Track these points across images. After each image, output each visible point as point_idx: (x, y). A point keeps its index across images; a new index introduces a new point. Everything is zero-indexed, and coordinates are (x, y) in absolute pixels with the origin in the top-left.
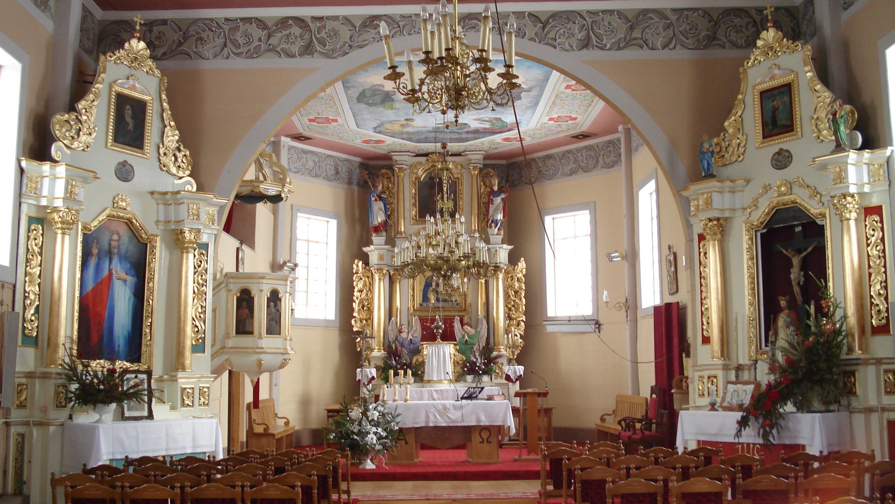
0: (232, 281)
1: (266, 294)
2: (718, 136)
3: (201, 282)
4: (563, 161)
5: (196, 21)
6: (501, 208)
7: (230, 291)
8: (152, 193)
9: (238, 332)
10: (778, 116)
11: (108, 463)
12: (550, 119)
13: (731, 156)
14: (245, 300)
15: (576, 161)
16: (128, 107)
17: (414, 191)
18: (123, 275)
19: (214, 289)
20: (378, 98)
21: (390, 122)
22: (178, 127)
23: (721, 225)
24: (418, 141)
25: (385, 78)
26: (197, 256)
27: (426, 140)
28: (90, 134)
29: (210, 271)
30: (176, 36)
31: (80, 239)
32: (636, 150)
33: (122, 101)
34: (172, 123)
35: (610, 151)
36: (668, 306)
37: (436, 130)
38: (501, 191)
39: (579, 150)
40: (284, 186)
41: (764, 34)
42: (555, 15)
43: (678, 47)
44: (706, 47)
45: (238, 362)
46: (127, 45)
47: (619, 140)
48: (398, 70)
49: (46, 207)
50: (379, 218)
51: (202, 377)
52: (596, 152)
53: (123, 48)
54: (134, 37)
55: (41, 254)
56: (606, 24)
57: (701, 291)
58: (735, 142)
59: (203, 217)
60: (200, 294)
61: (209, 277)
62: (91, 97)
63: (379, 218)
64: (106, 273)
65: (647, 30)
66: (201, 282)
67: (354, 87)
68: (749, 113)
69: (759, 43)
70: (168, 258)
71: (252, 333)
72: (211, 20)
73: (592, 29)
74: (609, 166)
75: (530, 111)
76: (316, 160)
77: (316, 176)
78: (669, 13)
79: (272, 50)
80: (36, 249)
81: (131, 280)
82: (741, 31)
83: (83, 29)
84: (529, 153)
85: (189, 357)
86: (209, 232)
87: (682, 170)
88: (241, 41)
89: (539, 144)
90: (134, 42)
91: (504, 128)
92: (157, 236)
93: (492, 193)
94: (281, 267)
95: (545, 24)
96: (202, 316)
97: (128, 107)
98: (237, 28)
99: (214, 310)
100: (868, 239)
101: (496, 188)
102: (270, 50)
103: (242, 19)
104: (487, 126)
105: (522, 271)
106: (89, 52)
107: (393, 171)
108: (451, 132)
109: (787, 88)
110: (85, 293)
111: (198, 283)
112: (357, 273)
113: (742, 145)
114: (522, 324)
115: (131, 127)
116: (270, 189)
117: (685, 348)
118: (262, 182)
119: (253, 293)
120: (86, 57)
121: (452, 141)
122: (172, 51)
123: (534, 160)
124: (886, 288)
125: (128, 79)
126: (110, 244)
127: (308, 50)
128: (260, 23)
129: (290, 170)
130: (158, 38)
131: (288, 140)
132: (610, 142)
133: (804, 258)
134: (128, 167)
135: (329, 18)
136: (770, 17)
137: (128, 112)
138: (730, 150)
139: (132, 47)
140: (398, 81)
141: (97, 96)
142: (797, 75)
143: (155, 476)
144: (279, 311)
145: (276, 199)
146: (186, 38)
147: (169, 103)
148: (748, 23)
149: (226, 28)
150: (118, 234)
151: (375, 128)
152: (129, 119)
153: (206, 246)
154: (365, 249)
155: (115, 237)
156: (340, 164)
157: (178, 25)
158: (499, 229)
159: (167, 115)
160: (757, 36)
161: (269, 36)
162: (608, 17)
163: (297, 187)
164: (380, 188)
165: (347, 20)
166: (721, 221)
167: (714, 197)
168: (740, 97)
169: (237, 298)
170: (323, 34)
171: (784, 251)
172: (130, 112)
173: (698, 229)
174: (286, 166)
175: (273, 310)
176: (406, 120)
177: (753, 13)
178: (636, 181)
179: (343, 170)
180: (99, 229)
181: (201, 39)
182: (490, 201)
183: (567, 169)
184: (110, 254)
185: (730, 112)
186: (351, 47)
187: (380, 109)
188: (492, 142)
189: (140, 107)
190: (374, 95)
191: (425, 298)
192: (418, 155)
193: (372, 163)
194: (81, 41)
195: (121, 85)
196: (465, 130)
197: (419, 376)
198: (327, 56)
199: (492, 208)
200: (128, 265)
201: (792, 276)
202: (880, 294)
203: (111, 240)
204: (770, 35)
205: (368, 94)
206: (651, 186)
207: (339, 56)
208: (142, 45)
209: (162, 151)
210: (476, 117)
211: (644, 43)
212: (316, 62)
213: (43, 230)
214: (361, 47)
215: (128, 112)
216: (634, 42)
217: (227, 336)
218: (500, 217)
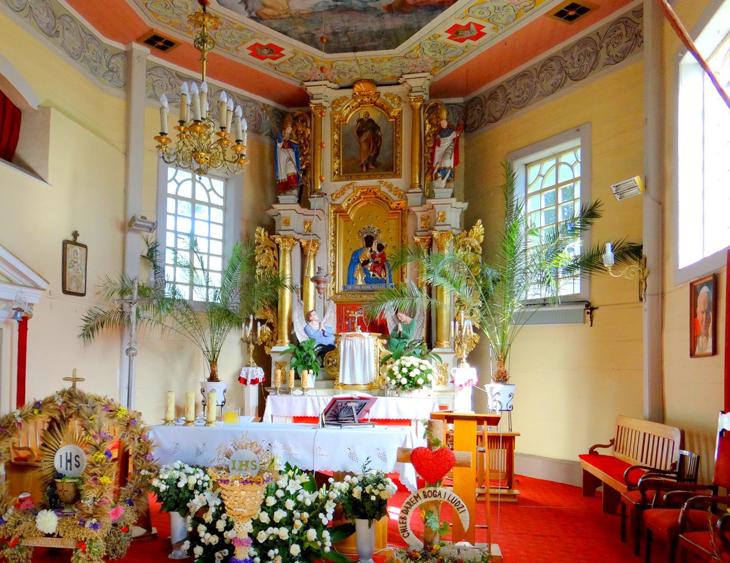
4: (542, 75)
15: (562, 68)
17: (336, 137)
25: (284, 49)
35: (620, 35)
39: (565, 52)
50: (287, 167)
84: (480, 83)
93: (441, 132)
101: (444, 124)
105: (478, 239)
112: (259, 244)
114: (477, 311)
123: (501, 87)
158: (448, 181)
182: (437, 143)
183: (548, 85)
191: (350, 279)
192: (341, 88)
199: (439, 151)
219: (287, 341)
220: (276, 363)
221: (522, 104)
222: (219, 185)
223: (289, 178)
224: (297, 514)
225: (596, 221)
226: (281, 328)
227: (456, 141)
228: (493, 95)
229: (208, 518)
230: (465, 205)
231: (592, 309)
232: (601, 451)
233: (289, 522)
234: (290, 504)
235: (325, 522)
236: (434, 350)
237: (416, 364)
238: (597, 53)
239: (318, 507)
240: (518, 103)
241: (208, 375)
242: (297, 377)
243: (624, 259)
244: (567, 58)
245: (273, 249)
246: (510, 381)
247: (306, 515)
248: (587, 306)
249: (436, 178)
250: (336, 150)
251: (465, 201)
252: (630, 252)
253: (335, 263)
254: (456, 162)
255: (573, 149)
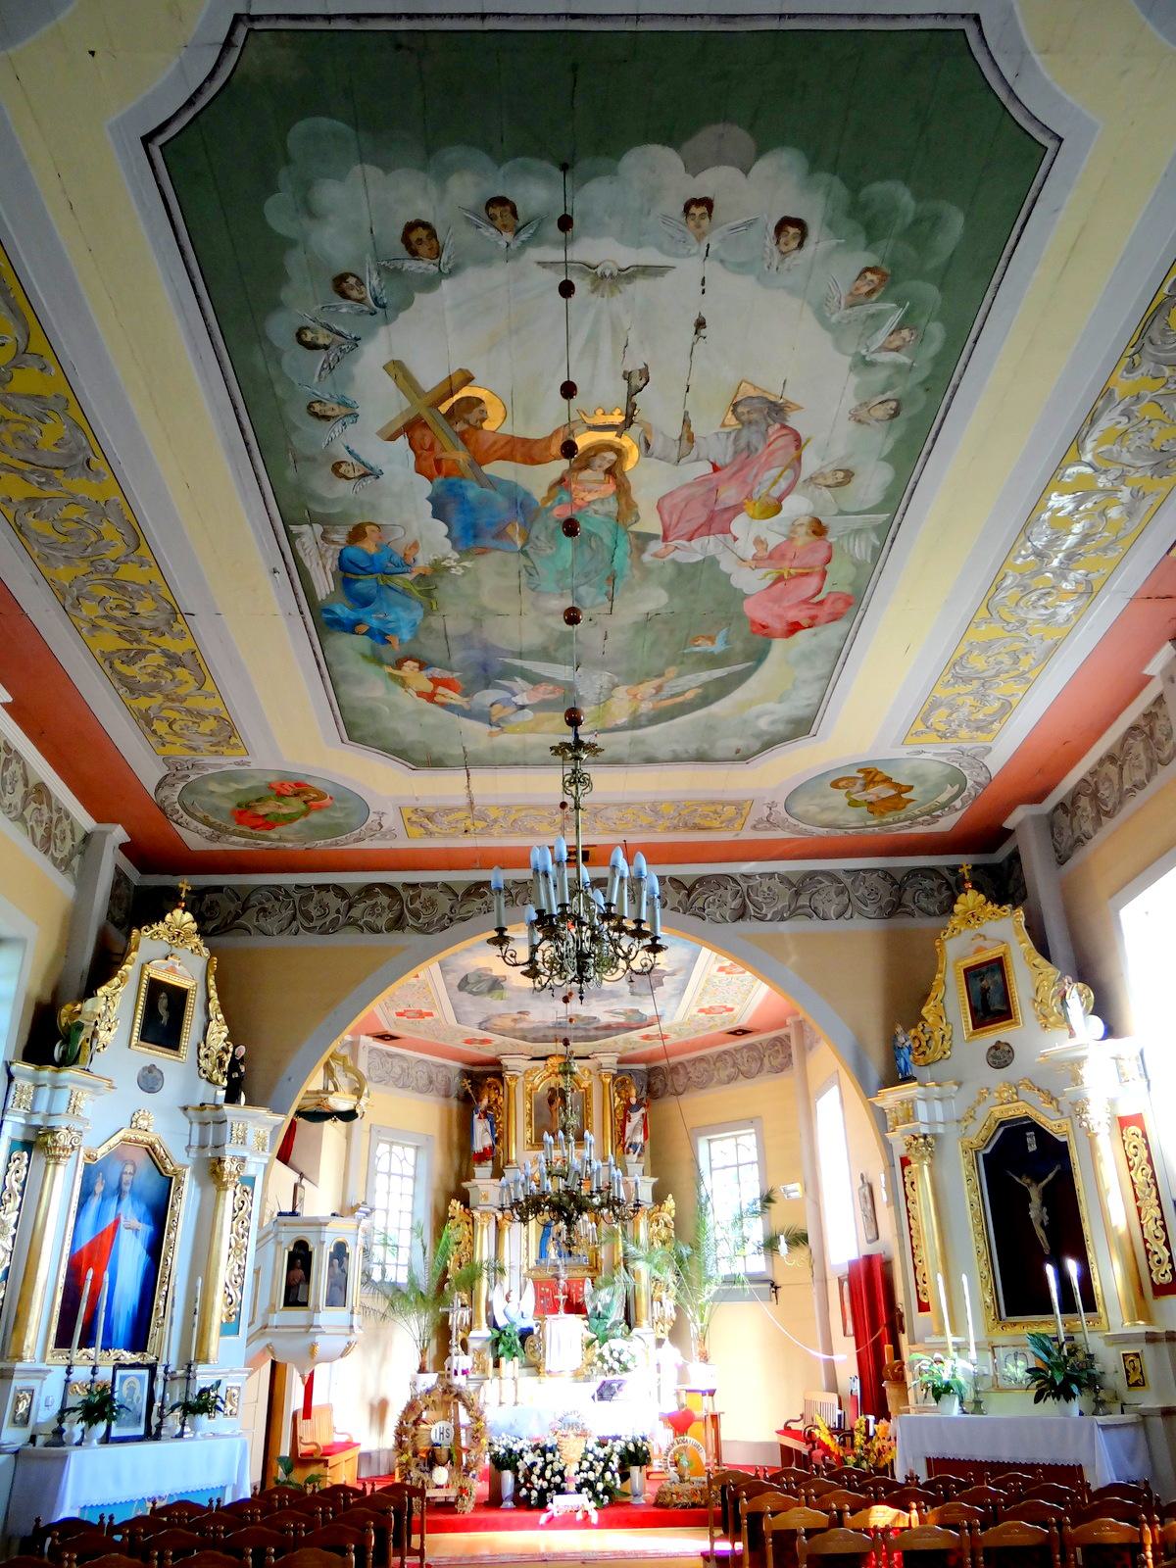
0: (283, 1229)
1: (329, 1248)
2: (916, 1027)
3: (241, 1231)
5: (258, 888)
6: (640, 1127)
7: (280, 1243)
8: (185, 1109)
9: (285, 1305)
10: (991, 1002)
11: (76, 1514)
12: (702, 1011)
13: (934, 1052)
14: (301, 1257)
15: (735, 1065)
16: (163, 995)
17: (528, 1106)
18: (135, 1223)
19: (258, 1242)
20: (484, 986)
21: (500, 1016)
22: (228, 1021)
23: (930, 1145)
24: (535, 1040)
26: (239, 1195)
27: (545, 1039)
28: (109, 1029)
29: (255, 1216)
30: (233, 907)
31: (80, 1173)
32: (810, 1049)
33: (156, 987)
34: (220, 1016)
35: (778, 1051)
36: (869, 1259)
37: (558, 1026)
38: (639, 1105)
40: (359, 1098)
41: (962, 898)
42: (701, 880)
43: (856, 915)
44: (890, 915)
45: (285, 1348)
46: (168, 916)
47: (788, 1037)
48: (506, 934)
49: (39, 1128)
51: (231, 1371)
52: (762, 1051)
53: (163, 921)
54: (178, 907)
55: (22, 1195)
56: (766, 889)
57: (911, 1237)
58: (937, 1035)
59: (251, 1139)
60: (238, 1249)
61: (253, 1224)
62: (116, 981)
63: (482, 1139)
64: (111, 1220)
65: (816, 896)
66: (241, 1231)
67: (454, 971)
68: (952, 1001)
69: (957, 908)
70: (198, 1197)
71: (305, 1304)
72: (279, 887)
73: (748, 894)
74: (779, 1070)
75: (674, 1001)
76: (405, 1065)
77: (404, 1087)
78: (842, 876)
79: (352, 923)
80: (17, 1186)
81: (146, 1229)
82: (933, 895)
83: (114, 897)
84: (673, 1055)
85: (215, 1342)
86: (258, 1160)
87: (875, 1069)
88: (314, 913)
89: (687, 1042)
90: (178, 912)
91: (642, 1023)
92: (186, 1167)
93: (628, 1108)
94: (353, 1210)
95: (690, 891)
96: (239, 1280)
97: (163, 995)
98: (310, 898)
99: (257, 1272)
100: (1128, 1159)
101: (633, 1101)
102: (349, 924)
103: (317, 887)
104: (622, 1019)
106: (118, 925)
107: (502, 1080)
108: (576, 1029)
109: (998, 965)
110: (77, 1249)
111: (238, 1234)
113: (947, 1037)
115: (164, 1021)
116: (341, 1102)
117: (895, 1324)
118: (332, 1093)
119: (311, 1247)
120: (113, 930)
121: (577, 1039)
122: (226, 925)
123: (681, 1063)
124: (1164, 1227)
125: (166, 959)
126: (121, 1179)
127: (397, 924)
128: (339, 890)
129: (371, 1079)
130: (209, 909)
131: (370, 1039)
132: (777, 1039)
133: (1044, 1188)
134: (155, 1073)
135: (424, 885)
136: (967, 877)
137: (163, 1002)
138: (932, 1044)
139: (175, 919)
140: (504, 948)
141: (123, 979)
142: (1008, 948)
143: (179, 1517)
144: (344, 1272)
145: (349, 1116)
146: (245, 909)
147: (218, 991)
148: (941, 885)
149: (297, 896)
150: (134, 1164)
151: (480, 1023)
152: (162, 1011)
153: (251, 1181)
154: (465, 1185)
155: (129, 1169)
156: (434, 1070)
157: (235, 892)
158: (639, 1155)
159: (214, 1004)
160: (954, 900)
161: (350, 907)
162: (767, 882)
163: (380, 1104)
164: (485, 1102)
165: (447, 887)
166: (929, 1139)
167: (923, 1103)
168: (938, 976)
169: (290, 1253)
170: (417, 905)
171: (1017, 1179)
172: (165, 1002)
173: (900, 1150)
174: (366, 1075)
175: (337, 1270)
176: (520, 1013)
177: (946, 873)
178: (812, 1088)
179: (440, 1080)
180: (108, 1158)
181: (264, 910)
182: (627, 1118)
183: (724, 1074)
184: (119, 1192)
185: (927, 995)
186: (451, 920)
187: (487, 999)
188: (627, 1041)
189: (178, 997)
190: (479, 982)
191: (543, 1252)
192: (534, 1059)
193: (477, 1069)
194: (109, 912)
195: (156, 968)
196: (595, 1025)
197: (535, 1367)
198: (420, 930)
199: (629, 1127)
200: (143, 1208)
201: (1032, 1214)
202: (1157, 1237)
203: (122, 1173)
204: (970, 899)
205: (471, 980)
206: (833, 1093)
207: (436, 930)
208: (188, 916)
209: (202, 1052)
210: (607, 1009)
211: (814, 912)
212: (408, 939)
213: (29, 1159)
214: (464, 920)
215: (163, 1002)
216: (800, 911)
217: (272, 1308)
218: (639, 1138)
219: (484, 1324)
220: (474, 1350)
221: (702, 1086)
222: (410, 1153)
223: (485, 1149)
224: (595, 1463)
225: (772, 1205)
226: (479, 1310)
227: (644, 1116)
228: (674, 1069)
229: (537, 1471)
230: (654, 1180)
231: (776, 1288)
232: (794, 1426)
233: (592, 1468)
234: (590, 1457)
235: (614, 1469)
236: (635, 1331)
237: (625, 1349)
238: (762, 1060)
239: (607, 1460)
240: (698, 1083)
241: (418, 1368)
242: (497, 1365)
243: (797, 1244)
244: (738, 1056)
245: (468, 1224)
246: (710, 1361)
247: (602, 1464)
248: (772, 1285)
249: (628, 1153)
250: (528, 1118)
251: (653, 1175)
252: (799, 1239)
253: (528, 1237)
254: (646, 1138)
255: (750, 1134)
